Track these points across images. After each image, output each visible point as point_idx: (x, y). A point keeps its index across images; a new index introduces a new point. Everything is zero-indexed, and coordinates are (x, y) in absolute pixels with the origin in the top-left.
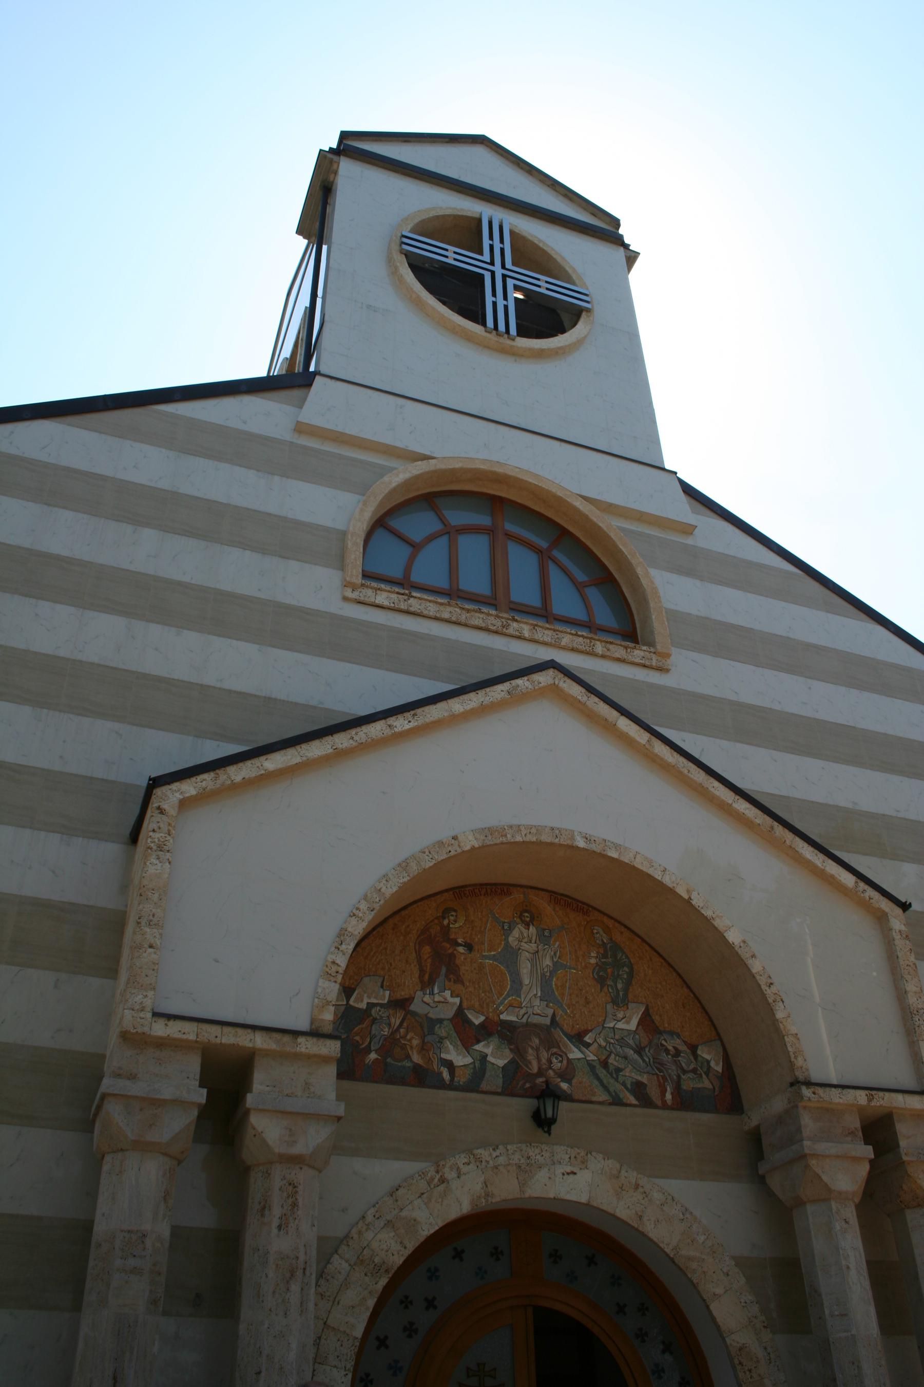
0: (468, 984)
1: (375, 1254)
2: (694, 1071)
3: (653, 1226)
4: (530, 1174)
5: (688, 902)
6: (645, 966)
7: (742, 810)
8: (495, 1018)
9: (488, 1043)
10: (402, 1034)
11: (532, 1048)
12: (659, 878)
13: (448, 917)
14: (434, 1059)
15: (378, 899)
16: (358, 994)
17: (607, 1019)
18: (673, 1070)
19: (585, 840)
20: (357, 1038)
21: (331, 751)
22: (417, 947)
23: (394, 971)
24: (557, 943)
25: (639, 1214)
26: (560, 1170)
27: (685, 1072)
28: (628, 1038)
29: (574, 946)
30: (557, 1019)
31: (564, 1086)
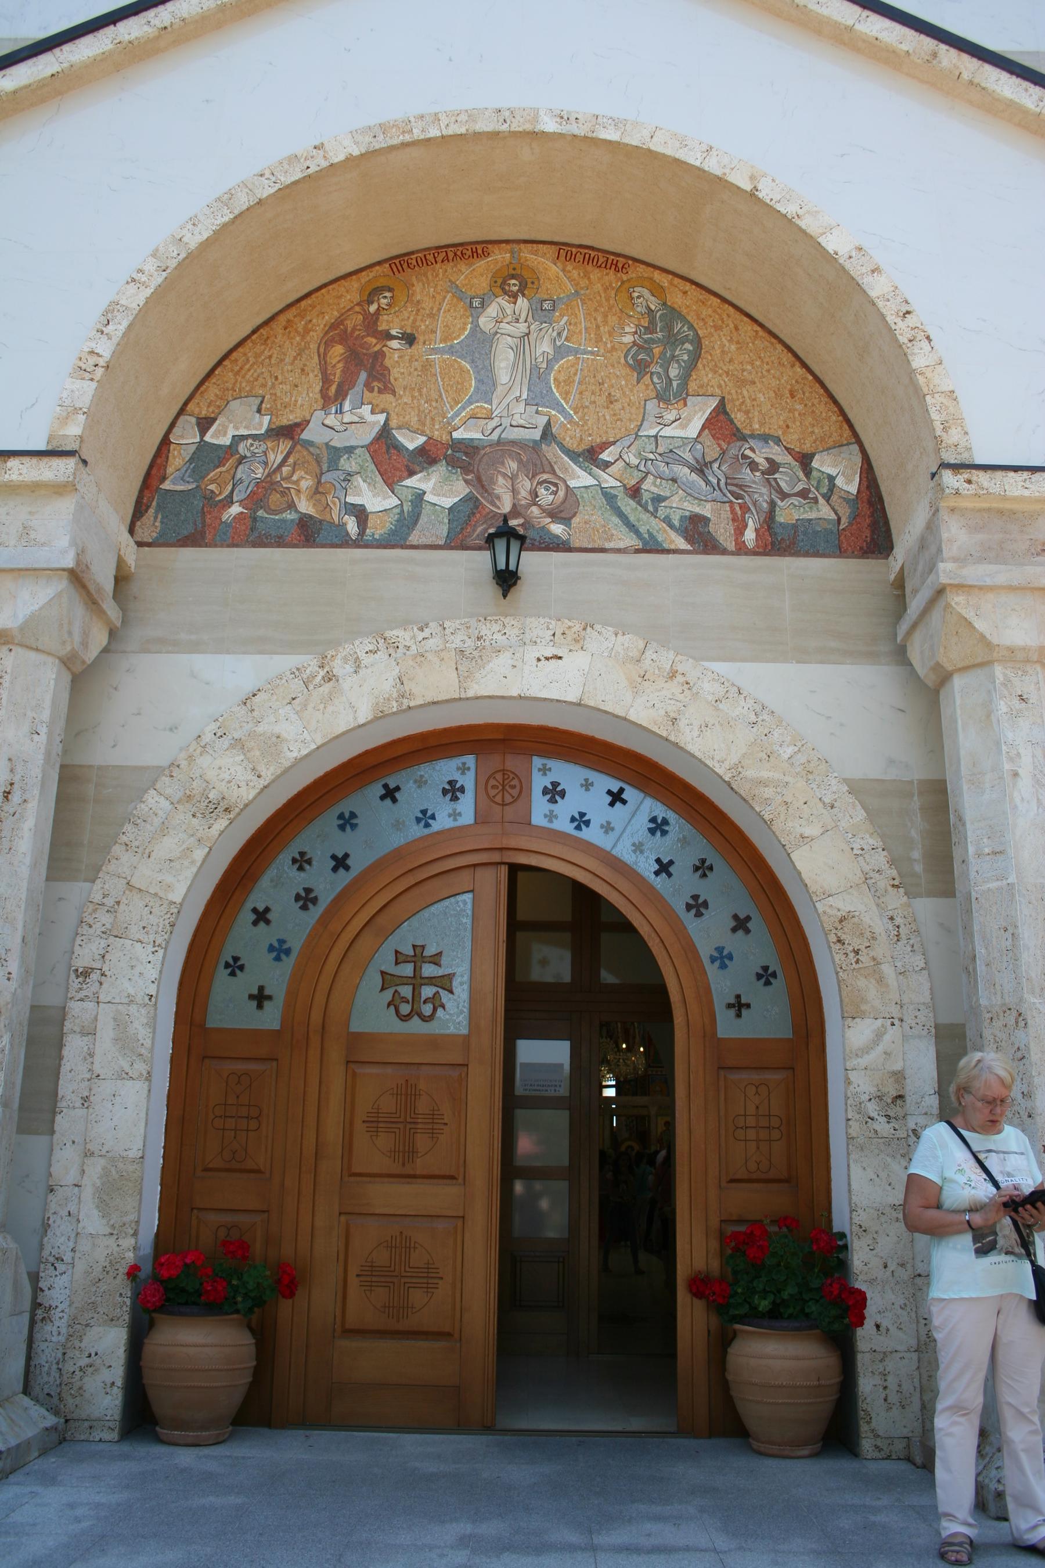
0: (401, 393)
1: (211, 787)
2: (804, 494)
3: (696, 733)
4: (479, 661)
5: (752, 196)
6: (723, 339)
7: (874, 34)
8: (444, 437)
9: (428, 475)
10: (284, 474)
11: (505, 475)
12: (697, 163)
13: (379, 299)
14: (335, 504)
15: (176, 252)
16: (219, 425)
17: (645, 423)
18: (762, 495)
19: (558, 120)
20: (212, 487)
21: (111, 46)
22: (322, 350)
23: (281, 386)
24: (565, 318)
25: (672, 715)
26: (533, 653)
27: (784, 496)
28: (682, 449)
29: (595, 319)
30: (554, 430)
31: (557, 529)
